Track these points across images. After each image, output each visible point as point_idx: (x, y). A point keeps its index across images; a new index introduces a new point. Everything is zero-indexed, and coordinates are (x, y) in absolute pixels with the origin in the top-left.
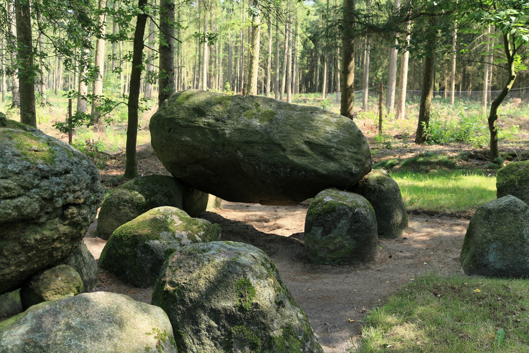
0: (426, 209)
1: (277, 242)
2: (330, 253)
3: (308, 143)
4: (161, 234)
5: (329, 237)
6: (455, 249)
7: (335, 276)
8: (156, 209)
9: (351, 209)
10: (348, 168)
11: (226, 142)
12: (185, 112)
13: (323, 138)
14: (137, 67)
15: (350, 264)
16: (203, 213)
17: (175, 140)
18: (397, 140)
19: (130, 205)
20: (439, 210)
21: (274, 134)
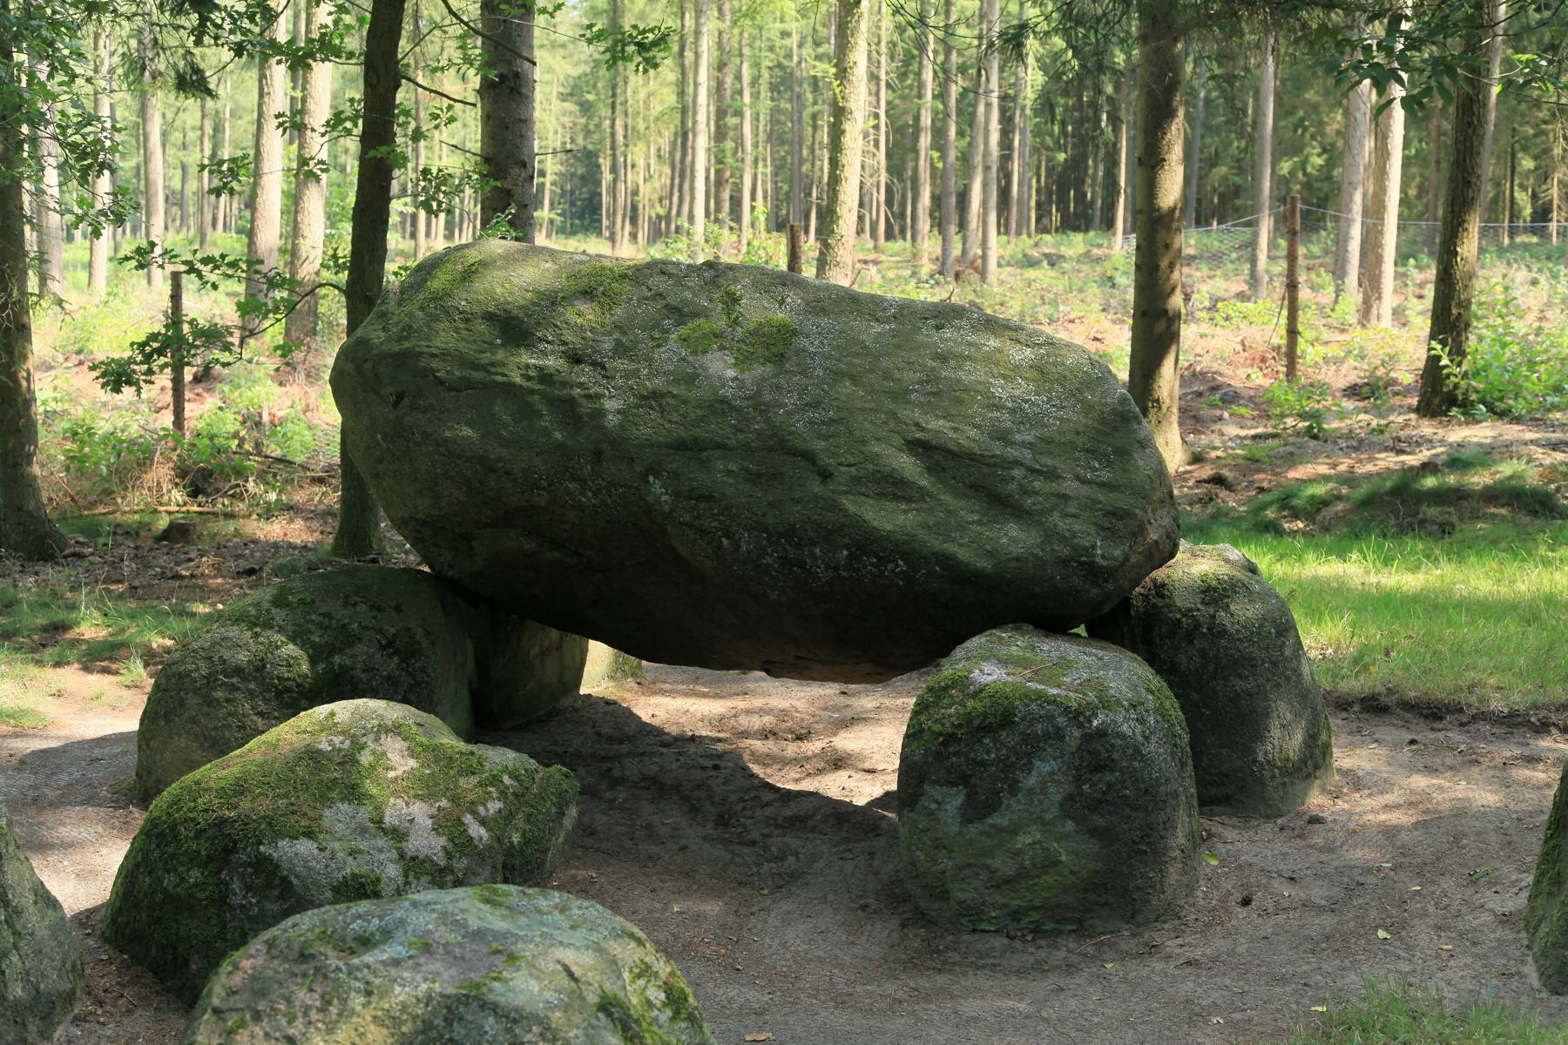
0: (1412, 694)
1: (813, 829)
2: (998, 887)
3: (922, 448)
4: (327, 813)
5: (993, 826)
6: (1509, 871)
7: (1012, 983)
8: (323, 710)
9: (1077, 716)
10: (1075, 548)
11: (609, 448)
12: (457, 330)
13: (978, 427)
14: (371, 154)
15: (1083, 931)
16: (567, 702)
17: (418, 438)
18: (1349, 404)
20: (1462, 698)
21: (788, 413)
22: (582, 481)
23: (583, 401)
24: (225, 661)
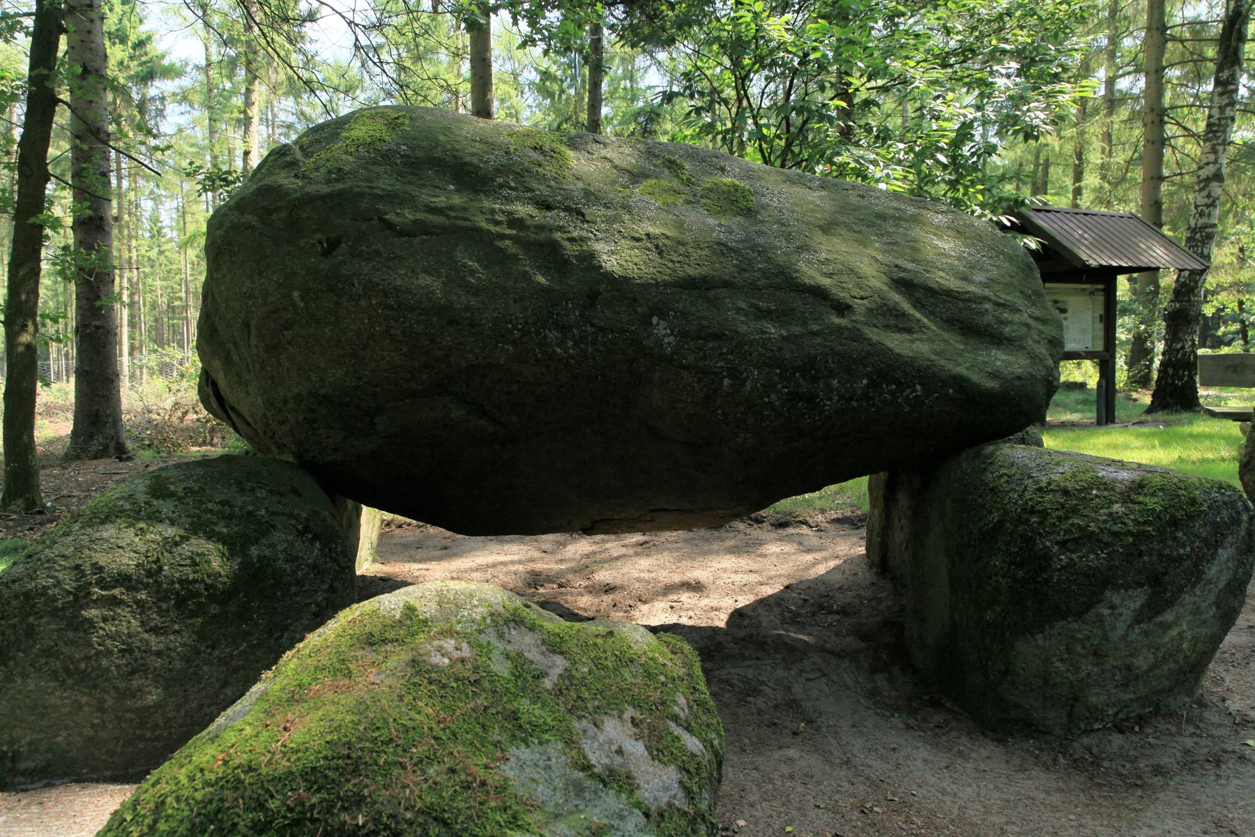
17: (358, 289)
19: (142, 595)
22: (564, 328)
23: (567, 244)
24: (101, 569)
